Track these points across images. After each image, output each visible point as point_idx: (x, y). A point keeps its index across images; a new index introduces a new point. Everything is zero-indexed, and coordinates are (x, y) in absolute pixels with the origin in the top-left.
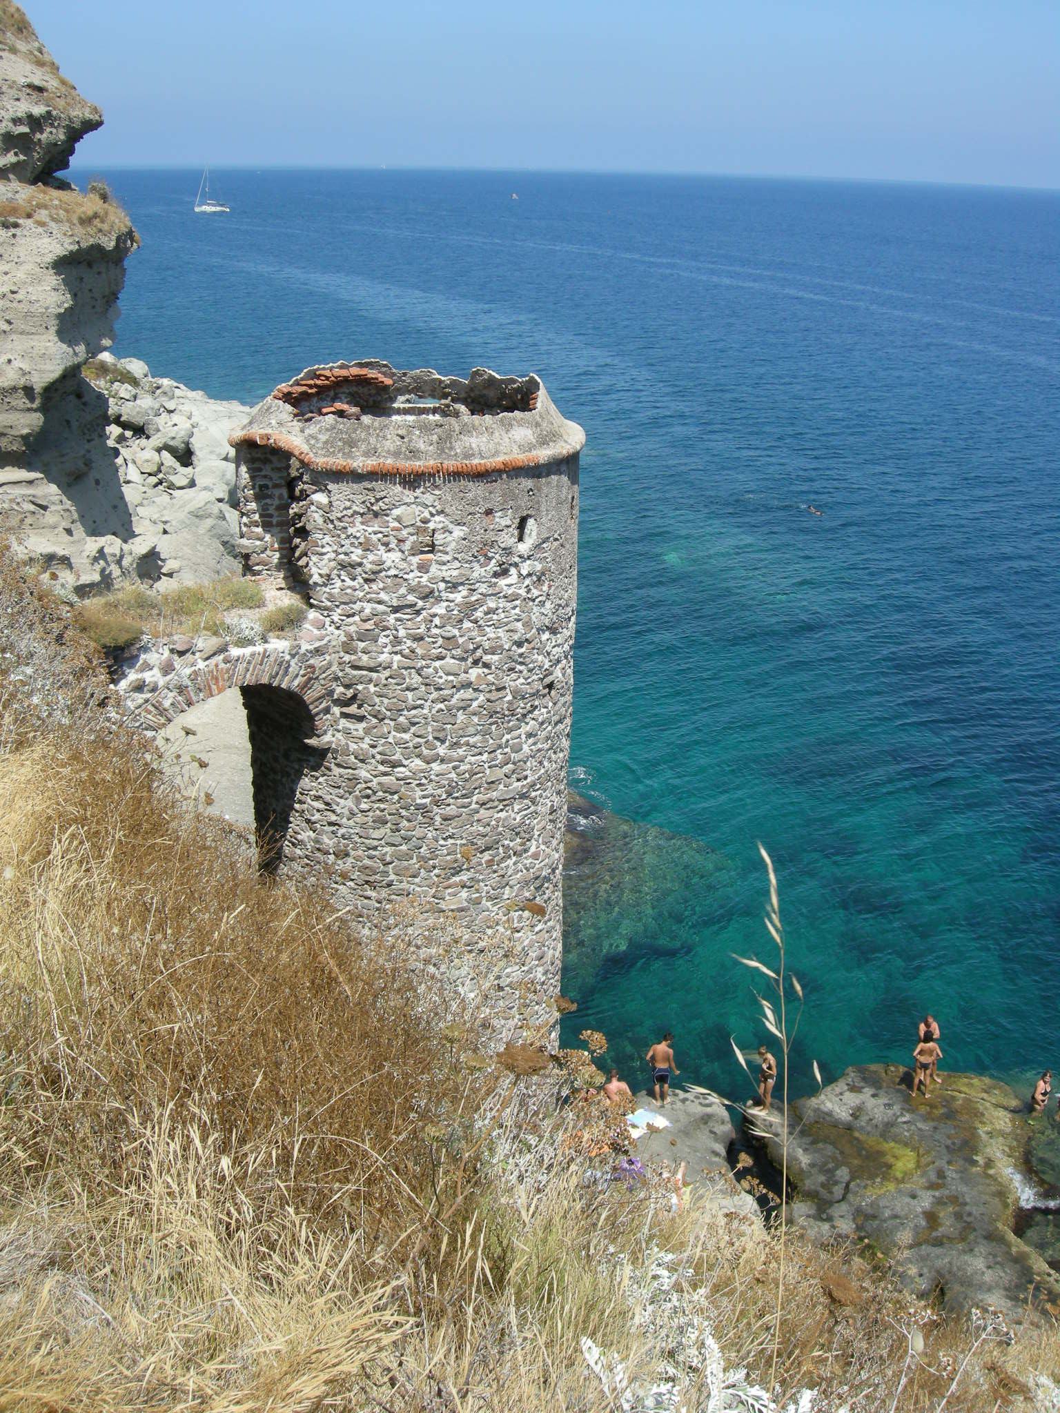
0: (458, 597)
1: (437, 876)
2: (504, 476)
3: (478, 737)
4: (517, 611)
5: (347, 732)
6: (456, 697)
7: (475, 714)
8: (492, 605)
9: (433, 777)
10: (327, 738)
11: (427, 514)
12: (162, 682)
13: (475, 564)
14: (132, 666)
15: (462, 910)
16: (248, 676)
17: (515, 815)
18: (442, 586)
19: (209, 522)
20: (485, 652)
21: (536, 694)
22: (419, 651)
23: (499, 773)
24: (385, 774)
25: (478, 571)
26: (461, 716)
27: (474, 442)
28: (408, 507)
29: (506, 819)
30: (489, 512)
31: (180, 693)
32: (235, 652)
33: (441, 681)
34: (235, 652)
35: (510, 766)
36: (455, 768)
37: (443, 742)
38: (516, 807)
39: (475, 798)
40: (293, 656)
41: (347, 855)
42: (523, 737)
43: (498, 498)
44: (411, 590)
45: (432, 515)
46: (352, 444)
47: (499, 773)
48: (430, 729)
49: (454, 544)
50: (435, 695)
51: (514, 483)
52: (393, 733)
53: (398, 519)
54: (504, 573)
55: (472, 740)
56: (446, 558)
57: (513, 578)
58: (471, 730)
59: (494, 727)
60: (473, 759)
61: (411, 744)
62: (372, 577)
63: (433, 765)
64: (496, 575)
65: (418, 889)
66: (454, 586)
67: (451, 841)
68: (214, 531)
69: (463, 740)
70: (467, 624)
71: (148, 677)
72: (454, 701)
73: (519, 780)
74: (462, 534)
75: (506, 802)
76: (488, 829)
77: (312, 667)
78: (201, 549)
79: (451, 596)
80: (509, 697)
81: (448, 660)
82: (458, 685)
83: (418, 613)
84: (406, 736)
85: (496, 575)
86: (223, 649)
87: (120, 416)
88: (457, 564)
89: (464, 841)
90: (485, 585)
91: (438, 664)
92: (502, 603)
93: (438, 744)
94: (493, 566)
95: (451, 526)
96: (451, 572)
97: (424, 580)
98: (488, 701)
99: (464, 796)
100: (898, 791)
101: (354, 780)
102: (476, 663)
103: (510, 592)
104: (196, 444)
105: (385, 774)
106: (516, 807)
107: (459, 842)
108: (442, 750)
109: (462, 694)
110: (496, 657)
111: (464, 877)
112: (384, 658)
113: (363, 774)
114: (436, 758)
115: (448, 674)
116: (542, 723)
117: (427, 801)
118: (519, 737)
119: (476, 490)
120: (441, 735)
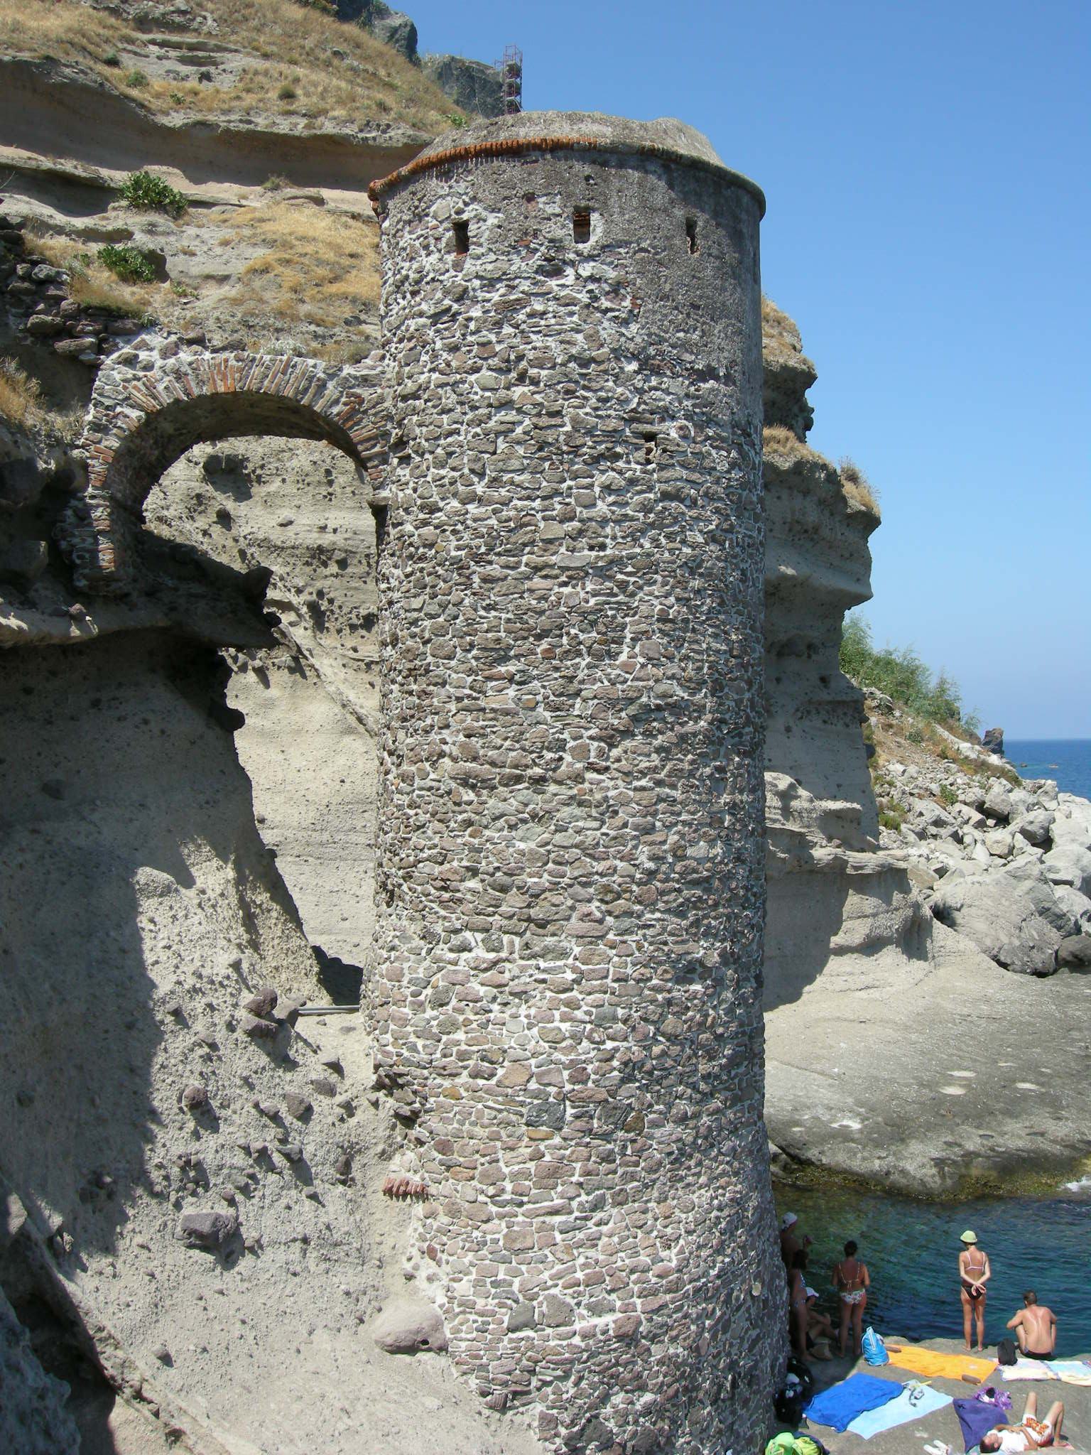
1: (477, 658)
3: (526, 476)
4: (575, 318)
6: (494, 419)
7: (519, 443)
8: (539, 307)
9: (469, 522)
11: (461, 205)
13: (514, 257)
14: (128, 342)
15: (507, 713)
16: (266, 383)
18: (477, 283)
19: (1028, 884)
23: (558, 530)
25: (517, 264)
29: (570, 595)
30: (530, 198)
31: (178, 379)
33: (476, 398)
35: (576, 524)
37: (481, 475)
39: (524, 559)
40: (331, 376)
42: (597, 490)
43: (539, 181)
45: (466, 204)
47: (558, 530)
48: (465, 461)
49: (488, 232)
50: (470, 416)
51: (562, 165)
52: (432, 470)
54: (557, 272)
55: (518, 479)
56: (480, 251)
58: (515, 464)
59: (547, 464)
60: (519, 503)
61: (446, 481)
62: (416, 288)
63: (470, 507)
65: (454, 675)
66: (490, 284)
67: (493, 613)
68: (1033, 895)
69: (506, 477)
70: (507, 330)
72: (492, 424)
73: (591, 548)
74: (496, 221)
75: (576, 575)
76: (544, 605)
77: (358, 396)
78: (1007, 903)
79: (488, 296)
80: (568, 428)
81: (484, 372)
82: (495, 403)
83: (454, 318)
87: (984, 803)
88: (492, 257)
89: (510, 616)
90: (528, 282)
91: (473, 378)
92: (552, 306)
93: (476, 479)
94: (536, 261)
95: (484, 214)
96: (488, 266)
98: (536, 427)
102: (522, 378)
103: (562, 294)
104: (1056, 831)
106: (589, 587)
107: (503, 616)
108: (480, 489)
109: (501, 416)
110: (544, 373)
111: (512, 667)
114: (474, 498)
115: (484, 389)
117: (463, 553)
118: (590, 486)
119: (511, 170)
120: (477, 467)
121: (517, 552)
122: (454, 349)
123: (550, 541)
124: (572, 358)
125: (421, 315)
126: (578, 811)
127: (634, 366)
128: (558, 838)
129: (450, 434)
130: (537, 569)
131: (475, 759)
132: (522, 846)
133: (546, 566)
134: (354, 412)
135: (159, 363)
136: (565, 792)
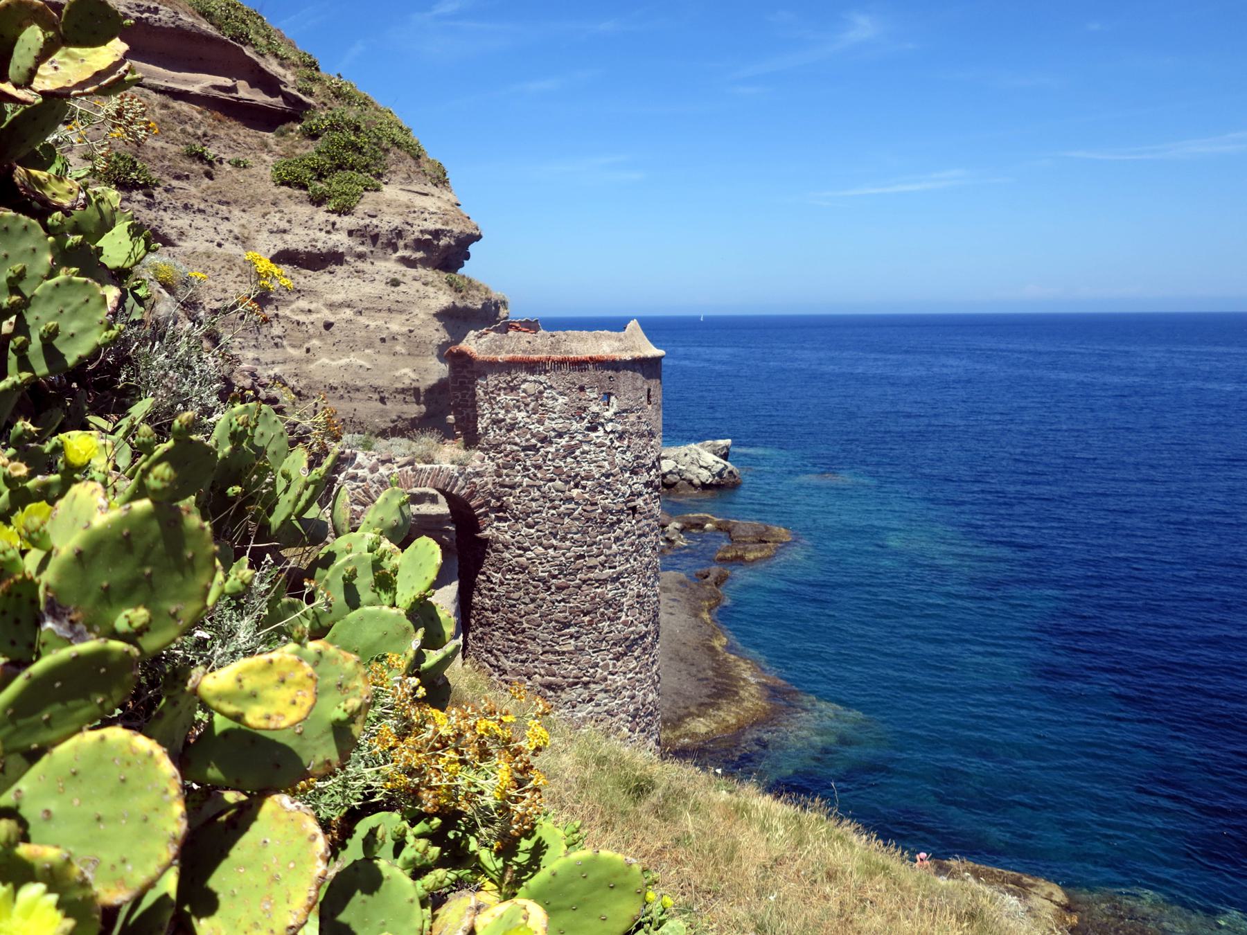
0: (563, 441)
2: (591, 367)
5: (498, 529)
10: (487, 532)
12: (370, 476)
17: (609, 591)
18: (553, 434)
20: (582, 478)
21: (621, 511)
22: (539, 475)
24: (520, 556)
25: (575, 426)
26: (567, 520)
27: (574, 345)
28: (529, 383)
30: (582, 389)
32: (420, 466)
34: (420, 466)
36: (564, 554)
38: (609, 587)
40: (461, 475)
41: (498, 610)
44: (533, 436)
46: (501, 347)
53: (524, 391)
54: (594, 429)
56: (553, 416)
57: (601, 432)
58: (574, 530)
64: (588, 429)
66: (560, 435)
71: (360, 472)
72: (562, 509)
75: (602, 582)
84: (532, 531)
85: (588, 429)
86: (411, 463)
92: (593, 448)
94: (585, 423)
96: (559, 425)
97: (541, 429)
99: (570, 574)
100: (987, 652)
101: (502, 560)
102: (576, 486)
105: (520, 556)
106: (609, 587)
108: (554, 542)
111: (572, 630)
112: (518, 479)
113: (506, 555)
116: (627, 533)
121: (574, 573)
122: (539, 467)
123: (591, 567)
124: (603, 475)
125: (516, 444)
126: (605, 695)
127: (627, 475)
128: (596, 709)
129: (537, 512)
130: (584, 582)
131: (554, 675)
132: (580, 715)
133: (590, 579)
134: (472, 492)
135: (370, 476)
136: (599, 687)
